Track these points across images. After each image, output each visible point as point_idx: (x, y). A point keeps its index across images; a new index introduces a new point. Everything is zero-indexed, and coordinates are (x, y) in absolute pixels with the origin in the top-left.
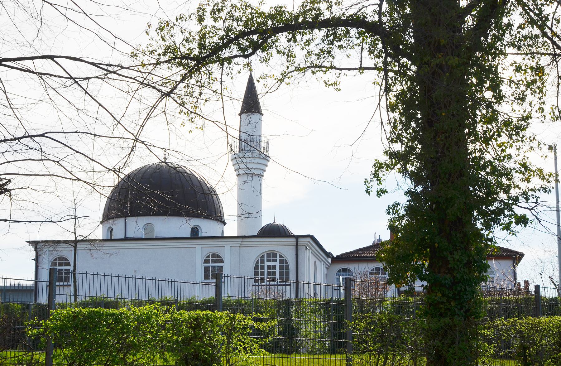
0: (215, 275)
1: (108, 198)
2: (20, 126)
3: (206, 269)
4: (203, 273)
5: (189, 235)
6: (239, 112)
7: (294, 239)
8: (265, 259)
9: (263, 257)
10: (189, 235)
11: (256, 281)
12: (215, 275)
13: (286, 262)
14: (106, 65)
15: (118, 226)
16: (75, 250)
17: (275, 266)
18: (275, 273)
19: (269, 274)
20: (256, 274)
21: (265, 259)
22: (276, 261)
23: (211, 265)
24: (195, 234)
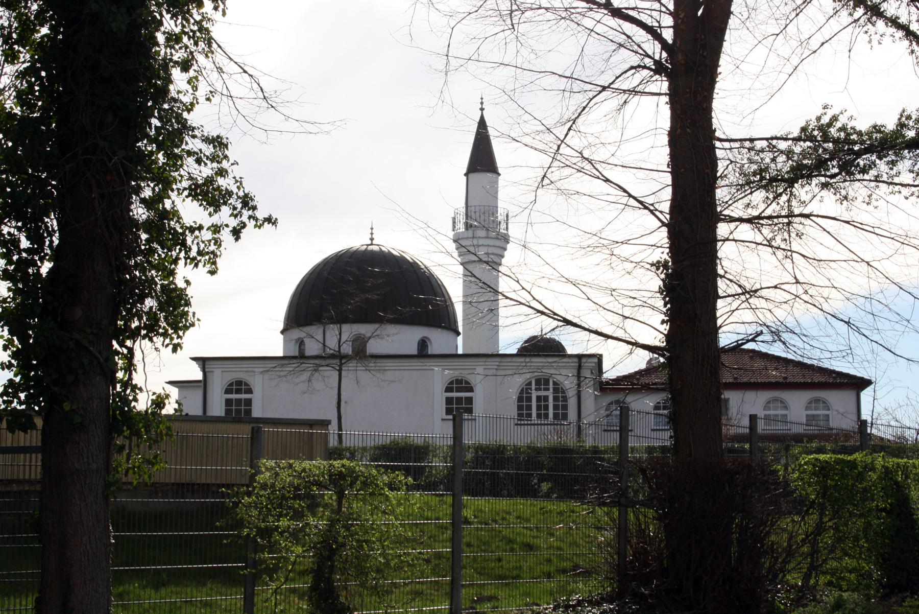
0: (459, 408)
2: (557, 295)
3: (449, 401)
4: (444, 406)
5: (415, 352)
6: (465, 171)
7: (576, 360)
8: (533, 387)
9: (530, 384)
10: (415, 352)
12: (459, 408)
15: (316, 339)
16: (340, 375)
17: (546, 398)
18: (546, 408)
19: (539, 408)
20: (520, 408)
21: (533, 387)
22: (548, 389)
23: (234, 396)
24: (423, 352)
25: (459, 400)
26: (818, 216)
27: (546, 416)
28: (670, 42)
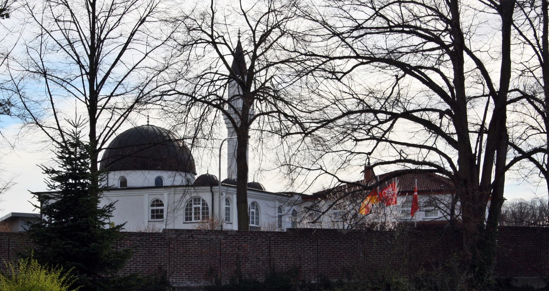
1: (148, 125)
3: (153, 211)
4: (150, 214)
5: (153, 184)
9: (191, 201)
10: (153, 184)
11: (187, 219)
13: (207, 205)
14: (84, 36)
17: (199, 208)
18: (195, 214)
22: (199, 204)
23: (155, 208)
25: (157, 210)
26: (137, 65)
27: (199, 219)
28: (439, 46)
